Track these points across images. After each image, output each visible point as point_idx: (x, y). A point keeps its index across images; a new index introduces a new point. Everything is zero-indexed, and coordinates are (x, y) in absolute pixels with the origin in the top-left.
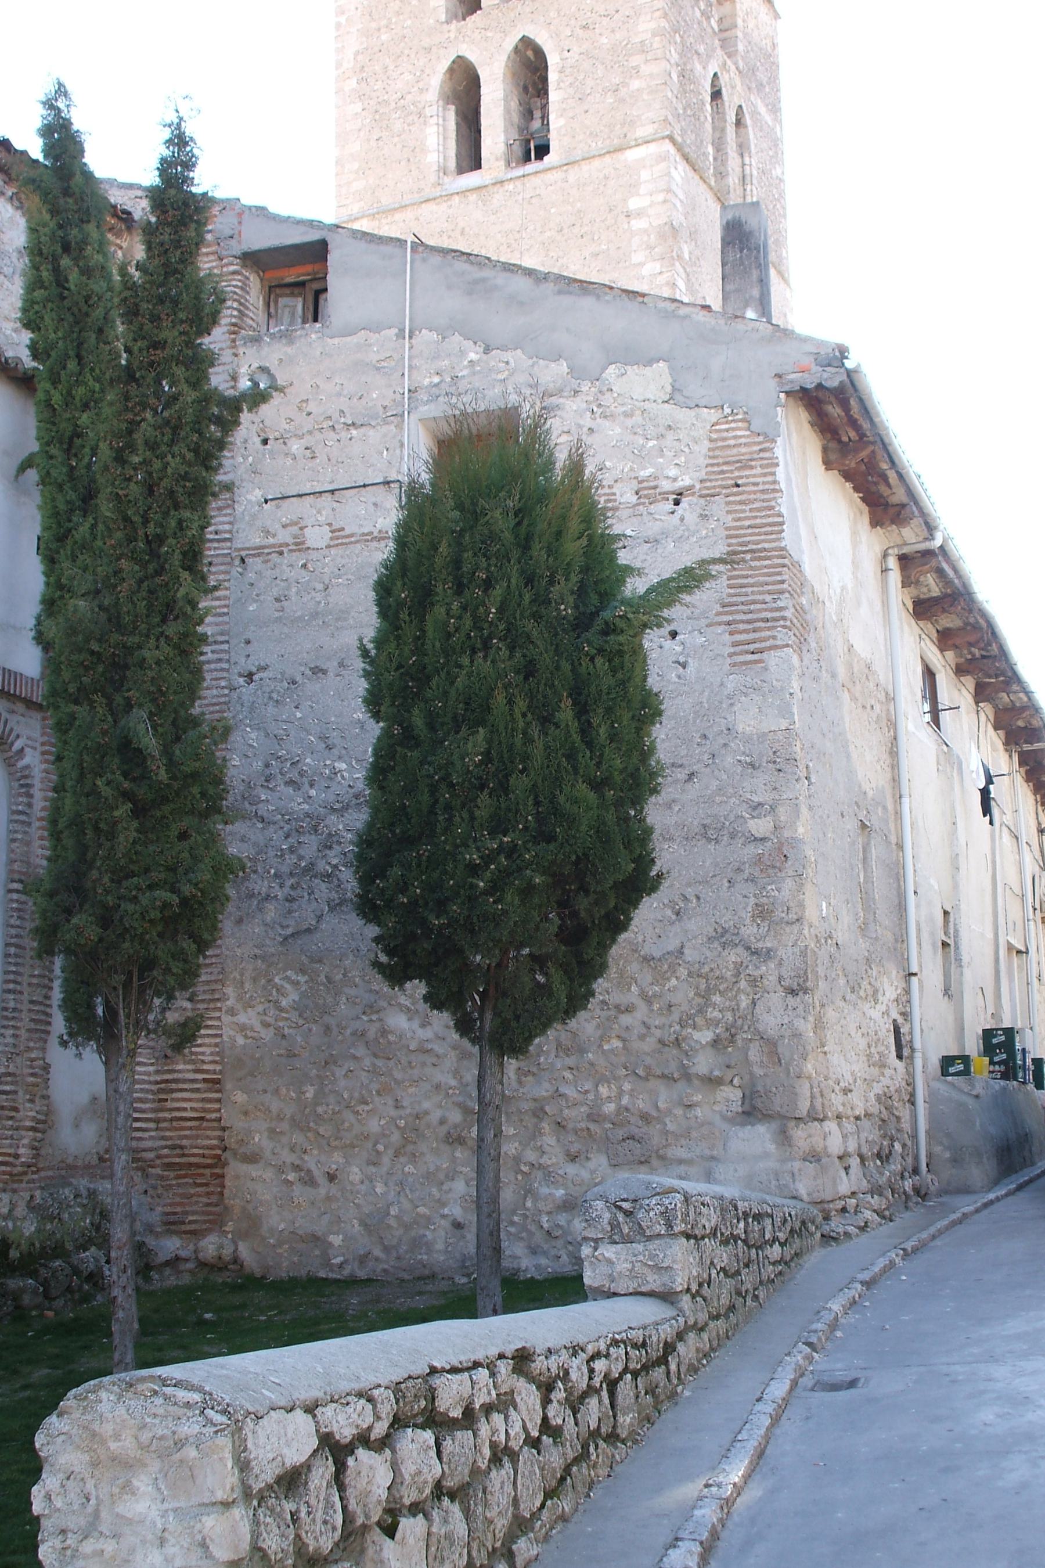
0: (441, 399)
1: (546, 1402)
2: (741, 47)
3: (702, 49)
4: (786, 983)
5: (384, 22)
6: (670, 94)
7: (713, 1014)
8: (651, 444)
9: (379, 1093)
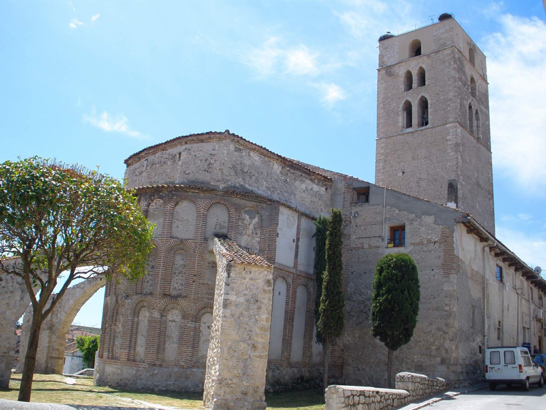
0: (391, 220)
1: (381, 398)
2: (477, 94)
3: (466, 97)
4: (450, 338)
5: (389, 91)
6: (457, 111)
7: (436, 344)
8: (430, 232)
9: (373, 354)
